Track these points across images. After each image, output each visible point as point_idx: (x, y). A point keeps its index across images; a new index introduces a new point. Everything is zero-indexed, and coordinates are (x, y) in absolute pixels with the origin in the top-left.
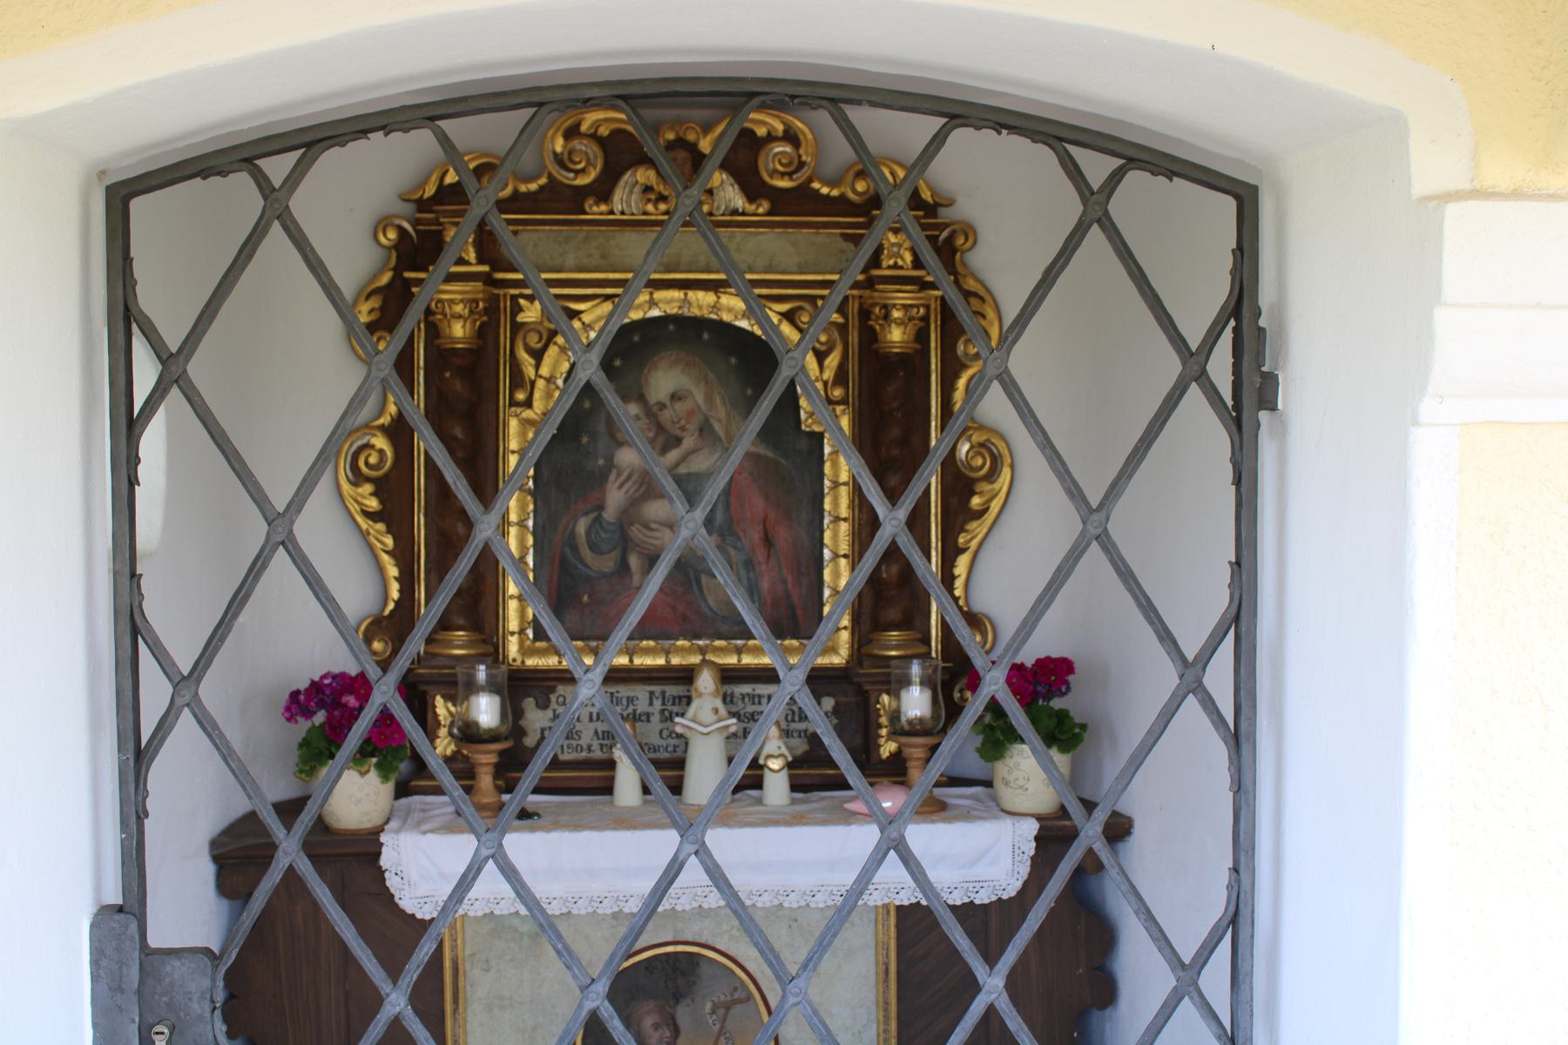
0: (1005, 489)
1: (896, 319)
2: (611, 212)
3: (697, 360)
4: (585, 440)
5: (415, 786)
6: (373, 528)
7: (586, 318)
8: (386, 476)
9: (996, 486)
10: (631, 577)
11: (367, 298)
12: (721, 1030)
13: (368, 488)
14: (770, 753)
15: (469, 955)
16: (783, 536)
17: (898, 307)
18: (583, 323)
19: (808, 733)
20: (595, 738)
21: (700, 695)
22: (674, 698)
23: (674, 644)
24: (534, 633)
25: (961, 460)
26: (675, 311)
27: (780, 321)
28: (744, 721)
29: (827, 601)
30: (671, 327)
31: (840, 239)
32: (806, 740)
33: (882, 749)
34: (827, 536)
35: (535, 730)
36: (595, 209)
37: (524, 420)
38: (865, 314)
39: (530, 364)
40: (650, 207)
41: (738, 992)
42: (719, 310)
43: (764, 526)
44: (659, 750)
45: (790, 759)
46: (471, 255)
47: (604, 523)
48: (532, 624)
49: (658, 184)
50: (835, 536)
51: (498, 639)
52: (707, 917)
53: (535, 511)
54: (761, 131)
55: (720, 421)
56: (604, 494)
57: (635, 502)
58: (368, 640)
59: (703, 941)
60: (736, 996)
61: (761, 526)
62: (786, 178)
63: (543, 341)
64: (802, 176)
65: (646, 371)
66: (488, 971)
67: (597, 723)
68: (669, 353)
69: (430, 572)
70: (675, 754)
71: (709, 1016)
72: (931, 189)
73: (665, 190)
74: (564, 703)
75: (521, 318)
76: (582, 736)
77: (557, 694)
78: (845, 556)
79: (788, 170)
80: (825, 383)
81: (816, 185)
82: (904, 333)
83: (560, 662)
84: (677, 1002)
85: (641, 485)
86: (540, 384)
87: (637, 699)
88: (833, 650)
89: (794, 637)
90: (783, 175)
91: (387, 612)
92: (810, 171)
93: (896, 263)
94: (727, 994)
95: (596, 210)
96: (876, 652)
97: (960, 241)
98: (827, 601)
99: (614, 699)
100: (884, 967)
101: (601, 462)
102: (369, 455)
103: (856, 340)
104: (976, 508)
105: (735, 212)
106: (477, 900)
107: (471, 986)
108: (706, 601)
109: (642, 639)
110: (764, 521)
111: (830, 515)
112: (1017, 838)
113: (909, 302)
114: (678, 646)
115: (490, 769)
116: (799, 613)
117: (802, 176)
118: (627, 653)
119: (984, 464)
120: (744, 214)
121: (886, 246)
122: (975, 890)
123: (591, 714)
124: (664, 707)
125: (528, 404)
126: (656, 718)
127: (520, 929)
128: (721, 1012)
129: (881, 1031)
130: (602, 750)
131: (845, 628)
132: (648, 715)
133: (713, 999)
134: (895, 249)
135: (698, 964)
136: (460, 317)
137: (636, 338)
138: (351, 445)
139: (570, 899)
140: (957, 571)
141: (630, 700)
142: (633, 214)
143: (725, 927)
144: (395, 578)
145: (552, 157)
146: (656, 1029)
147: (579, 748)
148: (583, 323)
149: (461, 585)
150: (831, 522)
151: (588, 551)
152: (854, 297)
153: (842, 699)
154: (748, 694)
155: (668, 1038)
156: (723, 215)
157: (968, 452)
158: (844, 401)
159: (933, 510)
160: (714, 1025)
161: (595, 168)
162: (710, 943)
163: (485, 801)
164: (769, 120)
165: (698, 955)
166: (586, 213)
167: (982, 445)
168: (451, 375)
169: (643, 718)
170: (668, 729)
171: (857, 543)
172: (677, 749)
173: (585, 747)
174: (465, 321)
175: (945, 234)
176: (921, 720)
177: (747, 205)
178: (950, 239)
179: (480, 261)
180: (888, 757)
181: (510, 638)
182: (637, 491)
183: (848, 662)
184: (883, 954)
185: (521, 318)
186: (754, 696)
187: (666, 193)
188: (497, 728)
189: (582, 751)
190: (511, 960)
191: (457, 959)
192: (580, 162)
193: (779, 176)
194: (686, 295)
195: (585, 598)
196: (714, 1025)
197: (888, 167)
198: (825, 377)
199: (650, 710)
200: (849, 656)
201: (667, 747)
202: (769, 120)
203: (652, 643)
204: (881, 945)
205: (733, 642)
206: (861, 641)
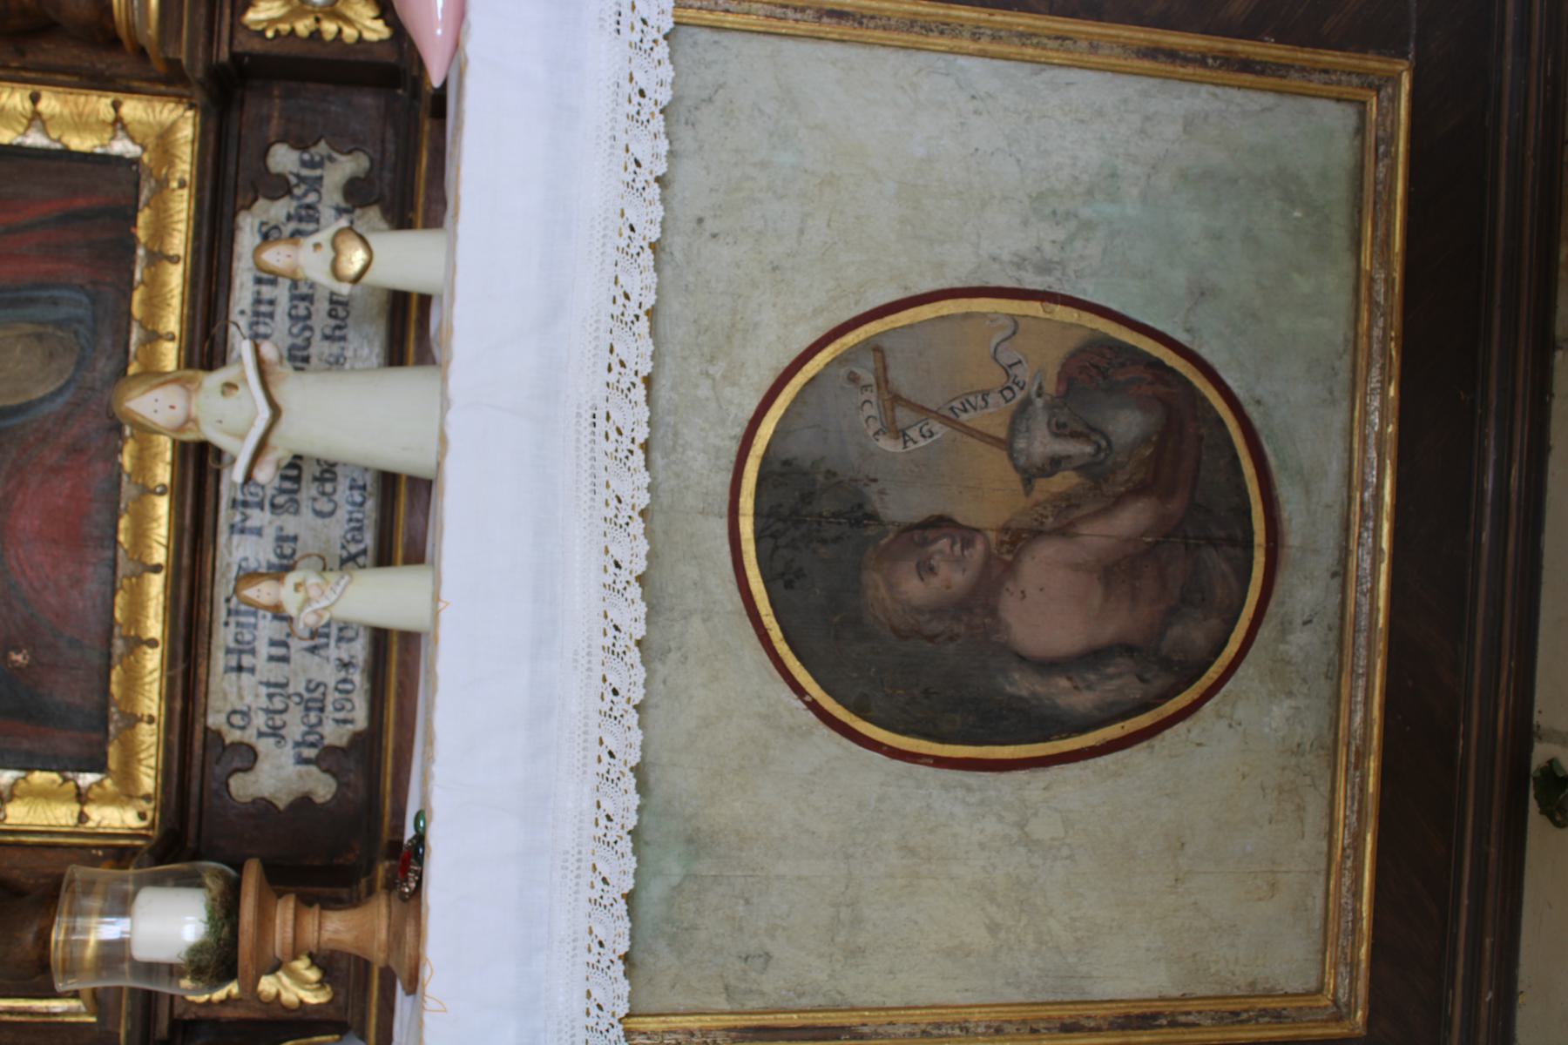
12: (945, 420)
14: (327, 268)
15: (729, 998)
19: (343, 205)
20: (322, 652)
21: (190, 420)
23: (129, 476)
24: (90, 770)
28: (308, 340)
29: (59, 140)
32: (358, 212)
33: (368, 36)
35: (301, 776)
41: (858, 371)
44: (358, 520)
48: (70, 775)
51: (97, 847)
52: (676, 434)
59: (734, 447)
60: (869, 378)
66: (768, 957)
67: (293, 650)
70: (369, 488)
71: (911, 446)
74: (245, 714)
76: (319, 679)
77: (225, 728)
83: (151, 720)
84: (873, 517)
87: (246, 559)
88: (164, 138)
89: (133, 220)
94: (864, 398)
100: (825, 20)
106: (589, 994)
107: (801, 995)
108: (42, 400)
109: (116, 542)
114: (134, 466)
115: (311, 919)
116: (81, 203)
118: (139, 576)
123: (272, 658)
126: (291, 524)
127: (675, 881)
128: (903, 416)
129: (973, 46)
130: (351, 640)
131: (116, 106)
132: (281, 539)
133: (871, 433)
135: (786, 463)
139: (602, 769)
143: (704, 391)
146: (932, 570)
147: (344, 683)
149: (112, 868)
153: (275, 127)
154: (252, 325)
155: (952, 546)
160: (932, 434)
162: (739, 431)
163: (383, 935)
165: (765, 460)
169: (287, 551)
170: (314, 499)
172: (360, 483)
173: (343, 674)
181: (90, 824)
183: (191, 107)
184: (797, 21)
186: (257, 314)
189: (351, 682)
190: (747, 902)
191: (734, 1029)
195: (18, 658)
196: (932, 434)
199: (270, 533)
200: (179, 103)
201: (354, 504)
203: (124, 523)
204: (775, 22)
205: (133, 348)
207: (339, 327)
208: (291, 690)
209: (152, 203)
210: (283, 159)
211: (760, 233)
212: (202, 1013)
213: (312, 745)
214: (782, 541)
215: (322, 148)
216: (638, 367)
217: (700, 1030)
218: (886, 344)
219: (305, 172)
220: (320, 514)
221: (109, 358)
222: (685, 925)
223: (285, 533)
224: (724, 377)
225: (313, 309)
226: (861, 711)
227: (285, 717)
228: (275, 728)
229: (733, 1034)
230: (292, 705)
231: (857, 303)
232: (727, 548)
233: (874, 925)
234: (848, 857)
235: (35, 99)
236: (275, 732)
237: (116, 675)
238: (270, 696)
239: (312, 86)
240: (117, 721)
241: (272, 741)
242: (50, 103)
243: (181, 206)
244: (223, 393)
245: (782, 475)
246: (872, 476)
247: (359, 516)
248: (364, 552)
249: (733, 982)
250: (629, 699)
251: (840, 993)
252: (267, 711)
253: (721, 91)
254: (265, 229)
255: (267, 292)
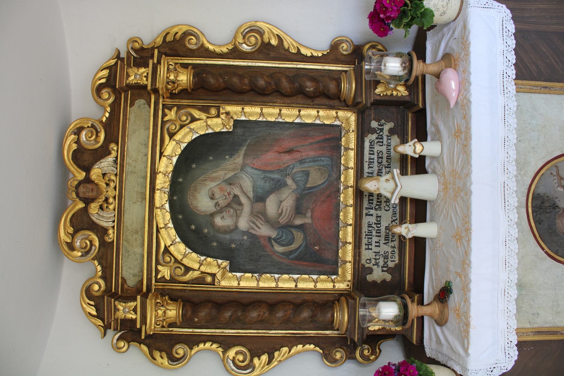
0: (268, 26)
1: (175, 77)
2: (113, 227)
3: (193, 184)
4: (233, 246)
5: (416, 341)
6: (277, 359)
7: (169, 243)
8: (249, 351)
9: (266, 30)
10: (307, 223)
11: (155, 359)
13: (256, 360)
14: (412, 151)
16: (288, 144)
17: (168, 76)
18: (171, 245)
19: (389, 135)
20: (388, 244)
21: (378, 189)
22: (369, 203)
25: (252, 49)
26: (166, 196)
27: (174, 140)
30: (175, 198)
31: (133, 107)
34: (288, 120)
36: (111, 236)
37: (222, 278)
38: (172, 96)
39: (193, 273)
40: (111, 207)
41: (553, 172)
42: (167, 172)
43: (282, 153)
45: (416, 140)
46: (133, 304)
47: (278, 237)
49: (99, 202)
50: (289, 116)
51: (336, 293)
53: (270, 273)
54: (75, 147)
55: (226, 174)
56: (263, 236)
57: (269, 222)
58: (334, 361)
59: (526, 191)
60: (555, 174)
61: (282, 154)
62: (99, 134)
63: (180, 266)
64: (99, 127)
65: (198, 212)
66: (538, 314)
68: (189, 200)
69: (301, 328)
72: (110, 60)
73: (341, 253)
74: (370, 260)
75: (168, 277)
77: (365, 263)
78: (299, 111)
79: (95, 133)
80: (208, 118)
81: (104, 119)
82: (183, 73)
84: (557, 207)
85: (259, 217)
86: (203, 269)
87: (369, 222)
88: (347, 119)
90: (97, 136)
91: (321, 351)
92: (96, 122)
93: (145, 76)
95: (112, 235)
96: (352, 95)
97: (137, 46)
98: (323, 122)
99: (369, 234)
100: (542, 89)
101: (245, 238)
102: (238, 360)
103: (186, 101)
104: (277, 42)
105: (115, 162)
107: (546, 323)
108: (320, 185)
110: (280, 153)
111: (277, 118)
112: (479, 5)
113: (166, 69)
116: (327, 137)
117: (99, 127)
119: (254, 36)
120: (117, 158)
121: (136, 82)
122: (507, 32)
123: (376, 246)
124: (374, 208)
125: (213, 275)
134: (138, 77)
135: (538, 194)
136: (165, 312)
137: (180, 217)
138: (233, 370)
140: (309, 55)
141: (370, 226)
142: (115, 216)
144: (303, 346)
145: (83, 258)
148: (171, 245)
150: (281, 118)
151: (292, 246)
152: (163, 101)
154: (369, 165)
156: (117, 168)
157: (248, 45)
158: (218, 108)
159: (277, 65)
161: (90, 235)
162: (527, 187)
164: (68, 143)
166: (113, 241)
167: (244, 37)
168: (197, 318)
170: (385, 207)
171: (292, 105)
174: (168, 309)
175: (133, 53)
176: (403, 63)
177: (112, 156)
178: (136, 51)
179: (135, 300)
180: (408, 92)
181: (336, 288)
182: (261, 219)
183: (354, 113)
185: (168, 277)
187: (104, 198)
188: (398, 304)
189: (394, 251)
190: (533, 300)
192: (86, 243)
193: (98, 138)
194: (158, 190)
197: (96, 81)
198: (204, 118)
199: (375, 215)
202: (68, 143)
203: (341, 214)
206: (345, 105)
207: (389, 165)
208: (380, 254)
209: (345, 136)
210: (374, 124)
211: (530, 140)
212: (372, 333)
213: (386, 267)
214: (538, 213)
215: (383, 121)
216: (514, 173)
217: (525, 332)
218: (558, 165)
219: (380, 127)
220: (386, 210)
221: (336, 174)
222: (520, 306)
223: (378, 215)
224: (523, 174)
225: (383, 160)
226: (556, 253)
227: (379, 260)
228: (377, 263)
229: (533, 333)
230: (381, 257)
231: (551, 156)
232: (526, 215)
233: (562, 306)
234: (555, 289)
235: (318, 112)
236: (377, 264)
237: (340, 251)
238: (376, 255)
239: (380, 106)
240: (340, 263)
241: (376, 266)
242: (322, 113)
243: (353, 137)
244: (386, 182)
245: (537, 197)
246: (557, 197)
247: (395, 210)
248: (396, 219)
249: (531, 320)
250: (515, 252)
251: (555, 323)
252: (375, 259)
253: (519, 107)
254: (371, 141)
255: (372, 156)
